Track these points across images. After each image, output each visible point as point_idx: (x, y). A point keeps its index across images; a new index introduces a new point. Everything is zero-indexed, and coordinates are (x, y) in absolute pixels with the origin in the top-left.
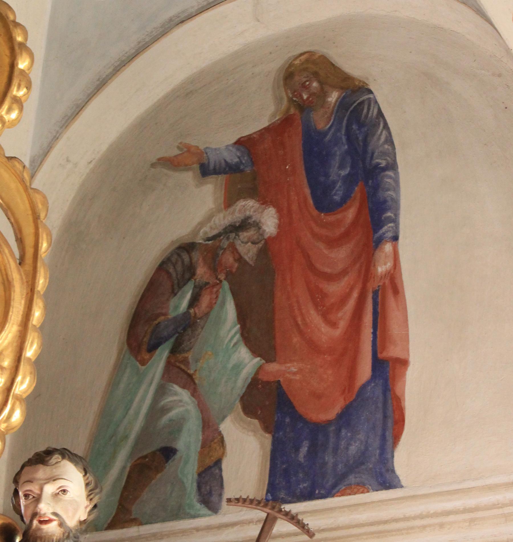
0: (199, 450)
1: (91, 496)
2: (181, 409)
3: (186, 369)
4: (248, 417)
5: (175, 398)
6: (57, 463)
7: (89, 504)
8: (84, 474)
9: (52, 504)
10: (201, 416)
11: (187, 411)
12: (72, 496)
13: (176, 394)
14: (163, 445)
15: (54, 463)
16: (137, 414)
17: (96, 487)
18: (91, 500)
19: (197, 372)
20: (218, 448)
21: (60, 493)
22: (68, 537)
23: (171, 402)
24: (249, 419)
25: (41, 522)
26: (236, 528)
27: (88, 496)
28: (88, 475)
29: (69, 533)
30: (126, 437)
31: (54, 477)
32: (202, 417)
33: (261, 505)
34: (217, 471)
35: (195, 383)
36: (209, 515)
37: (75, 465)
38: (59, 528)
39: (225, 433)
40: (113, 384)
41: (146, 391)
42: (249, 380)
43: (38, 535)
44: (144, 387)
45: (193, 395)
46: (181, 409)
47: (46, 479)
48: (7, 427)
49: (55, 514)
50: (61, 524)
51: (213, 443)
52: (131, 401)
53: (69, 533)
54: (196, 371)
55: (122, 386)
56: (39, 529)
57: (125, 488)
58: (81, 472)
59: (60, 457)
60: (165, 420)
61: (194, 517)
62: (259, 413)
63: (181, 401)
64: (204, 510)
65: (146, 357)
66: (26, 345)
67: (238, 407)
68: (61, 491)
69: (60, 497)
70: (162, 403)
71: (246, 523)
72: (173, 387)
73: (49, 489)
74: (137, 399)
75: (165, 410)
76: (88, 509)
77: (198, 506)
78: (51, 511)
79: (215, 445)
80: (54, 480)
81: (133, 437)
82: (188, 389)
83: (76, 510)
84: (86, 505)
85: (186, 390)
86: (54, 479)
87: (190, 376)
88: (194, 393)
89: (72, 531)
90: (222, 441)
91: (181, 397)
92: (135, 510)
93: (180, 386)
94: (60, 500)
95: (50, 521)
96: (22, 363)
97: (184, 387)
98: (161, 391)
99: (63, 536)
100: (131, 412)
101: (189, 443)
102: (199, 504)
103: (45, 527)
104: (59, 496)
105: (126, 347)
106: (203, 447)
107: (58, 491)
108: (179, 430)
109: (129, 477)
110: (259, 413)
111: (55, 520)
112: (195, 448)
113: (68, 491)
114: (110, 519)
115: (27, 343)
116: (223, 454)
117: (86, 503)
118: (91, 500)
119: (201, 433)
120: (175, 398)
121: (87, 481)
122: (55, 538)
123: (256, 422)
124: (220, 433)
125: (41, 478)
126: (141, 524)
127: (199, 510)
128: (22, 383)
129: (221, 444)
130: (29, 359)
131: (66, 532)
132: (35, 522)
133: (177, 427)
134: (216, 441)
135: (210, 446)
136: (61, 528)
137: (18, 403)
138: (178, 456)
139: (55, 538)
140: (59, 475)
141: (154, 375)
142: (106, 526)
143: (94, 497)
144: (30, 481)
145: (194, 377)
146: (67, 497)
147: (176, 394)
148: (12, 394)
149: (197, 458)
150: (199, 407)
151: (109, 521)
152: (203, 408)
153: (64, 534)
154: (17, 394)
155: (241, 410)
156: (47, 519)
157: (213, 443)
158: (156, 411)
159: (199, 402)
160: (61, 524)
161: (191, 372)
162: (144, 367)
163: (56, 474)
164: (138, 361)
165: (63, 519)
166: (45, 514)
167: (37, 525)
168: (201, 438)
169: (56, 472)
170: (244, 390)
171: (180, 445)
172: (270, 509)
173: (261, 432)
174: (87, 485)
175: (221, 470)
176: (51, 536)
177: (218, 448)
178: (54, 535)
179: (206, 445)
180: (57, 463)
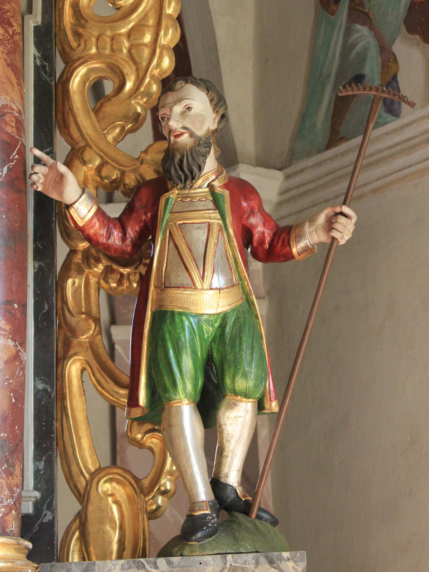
0: (380, 71)
1: (217, 109)
2: (364, 42)
3: (363, 10)
4: (411, 34)
5: (359, 34)
6: (181, 88)
7: (216, 115)
8: (207, 92)
9: (180, 121)
10: (378, 44)
11: (368, 42)
12: (197, 111)
13: (358, 31)
14: (355, 74)
15: (179, 88)
16: (334, 54)
17: (219, 101)
18: (217, 112)
19: (371, 9)
20: (393, 66)
21: (186, 111)
22: (199, 145)
23: (355, 39)
24: (412, 36)
25: (177, 136)
26: (414, 126)
27: (214, 109)
28: (210, 92)
29: (199, 141)
30: (329, 76)
31: (178, 100)
32: (379, 45)
33: (367, 90)
34: (395, 84)
35: (370, 19)
36: (394, 120)
37: (197, 87)
38: (190, 139)
39: (396, 53)
40: (315, 36)
41: (338, 35)
42: (409, 5)
43: (175, 147)
44: (336, 32)
45: (370, 29)
46: (364, 42)
47: (174, 102)
48: (159, 72)
49: (184, 128)
50: (192, 135)
51: (389, 60)
52: (328, 47)
53: (199, 141)
54: (370, 9)
55: (321, 36)
56: (176, 143)
57: (334, 115)
58: (203, 91)
59: (183, 83)
60: (354, 53)
61: (383, 125)
62: (419, 29)
63: (362, 36)
64: (390, 117)
65: (334, 9)
66: (165, 4)
67: (403, 28)
68: (187, 109)
69: (187, 114)
70: (350, 41)
71: (420, 120)
72: (355, 26)
73: (178, 109)
74: (333, 44)
75: (353, 46)
76: (217, 121)
77: (385, 115)
78: (180, 126)
79: (391, 64)
80: (180, 101)
81: (333, 74)
82: (366, 25)
83: (202, 122)
84: (214, 117)
85: (365, 26)
86: (179, 101)
87: (366, 14)
88: (371, 28)
89: (202, 139)
90: (395, 59)
91: (362, 31)
92: (343, 131)
93: (360, 25)
94: (187, 116)
95: (182, 134)
96: (163, 20)
97: (363, 24)
98: (348, 32)
99: (195, 144)
100: (330, 54)
101: (372, 69)
102: (385, 114)
103: (179, 140)
104: (186, 114)
105: (319, 4)
106: (382, 68)
107: (184, 110)
108: (364, 59)
109: (335, 106)
110: (419, 29)
111: (186, 133)
112: (377, 69)
113: (192, 108)
114: (327, 141)
115: (165, 2)
116: (398, 68)
117: (214, 115)
118: (217, 112)
119: (380, 57)
120: (359, 34)
121: (211, 98)
122: (188, 147)
123: (417, 37)
124: (393, 54)
125: (171, 102)
126: (348, 140)
127: (386, 118)
128: (166, 34)
129: (395, 62)
130: (170, 16)
131: (196, 140)
132: (172, 138)
133: (362, 57)
134: (391, 60)
135: (388, 66)
136: (192, 138)
137: (165, 51)
138: (366, 79)
139: (188, 147)
140: (183, 97)
141: (342, 21)
142: (324, 148)
143: (219, 109)
144: (163, 107)
145: (369, 14)
146: (193, 112)
147: (358, 31)
148: (158, 45)
149: (379, 78)
150: (376, 37)
151: (326, 144)
152: (378, 37)
153: (195, 143)
154: (164, 45)
155: (405, 31)
156: (179, 133)
157: (389, 63)
158: (347, 48)
159: (375, 33)
160: (192, 135)
161: (366, 11)
162: (334, 17)
163: (181, 96)
164: (329, 13)
165: (192, 130)
166: (176, 129)
167: (174, 140)
168: (380, 61)
169: (181, 94)
170: (406, 14)
171: (367, 71)
172: (375, 91)
173: (422, 44)
174: (211, 101)
175: (397, 82)
176: (185, 146)
177: (393, 66)
178: (187, 145)
179: (385, 66)
180: (181, 88)
